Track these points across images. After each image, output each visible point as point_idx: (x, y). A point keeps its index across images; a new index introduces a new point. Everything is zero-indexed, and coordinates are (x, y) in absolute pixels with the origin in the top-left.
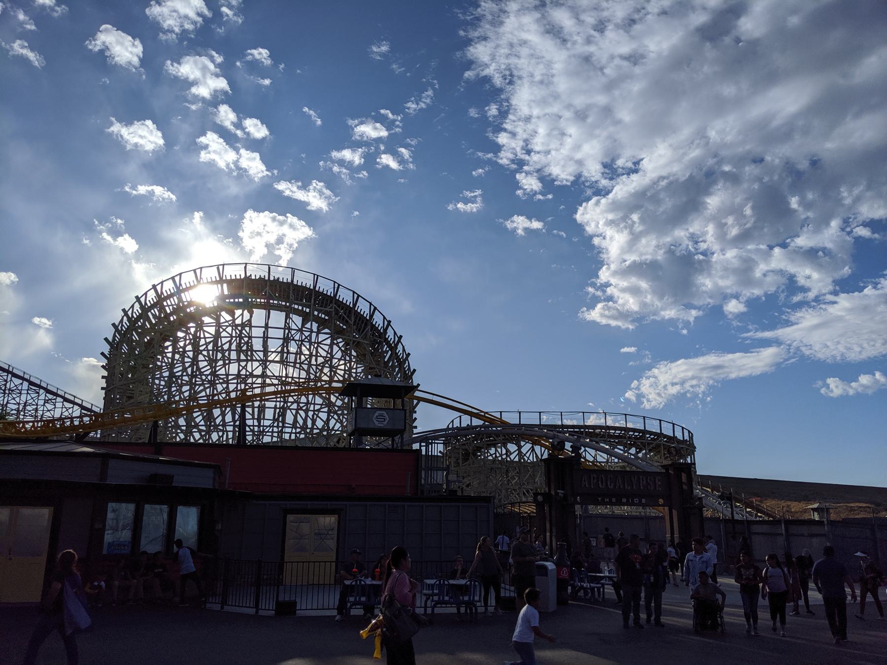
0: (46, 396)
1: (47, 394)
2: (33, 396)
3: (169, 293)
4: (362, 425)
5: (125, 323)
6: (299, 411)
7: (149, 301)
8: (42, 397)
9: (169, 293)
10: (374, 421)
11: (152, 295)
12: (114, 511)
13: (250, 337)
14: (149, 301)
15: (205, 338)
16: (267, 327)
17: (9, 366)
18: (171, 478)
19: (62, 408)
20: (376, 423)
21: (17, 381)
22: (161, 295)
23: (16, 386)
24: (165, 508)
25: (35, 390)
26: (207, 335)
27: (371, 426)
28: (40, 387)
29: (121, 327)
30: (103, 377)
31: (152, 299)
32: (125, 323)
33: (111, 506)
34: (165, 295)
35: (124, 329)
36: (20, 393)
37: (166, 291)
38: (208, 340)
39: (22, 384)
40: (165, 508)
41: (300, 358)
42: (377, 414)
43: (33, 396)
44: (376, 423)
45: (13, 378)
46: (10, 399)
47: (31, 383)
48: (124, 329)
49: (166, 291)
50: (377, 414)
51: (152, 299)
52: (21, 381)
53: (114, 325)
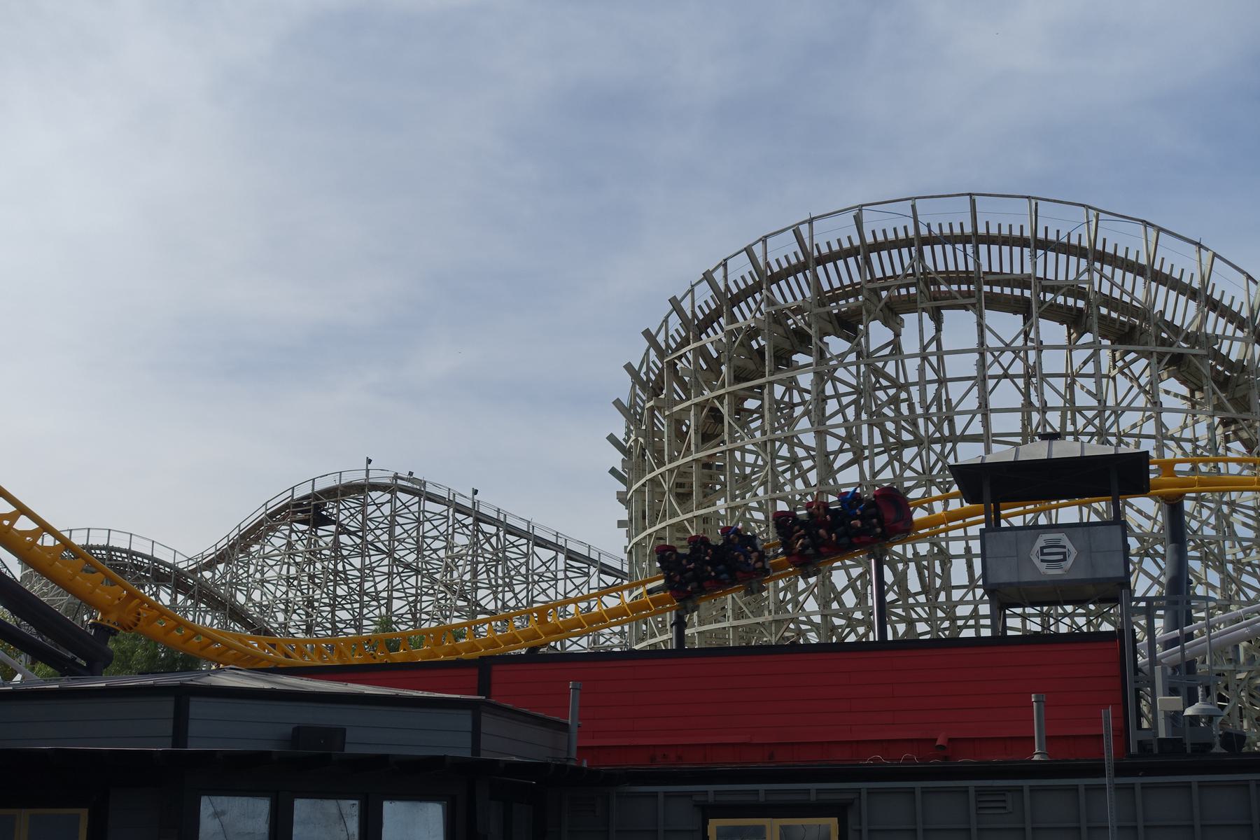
0: (600, 579)
1: (602, 576)
2: (578, 581)
3: (743, 286)
4: (1003, 575)
5: (677, 331)
6: (445, 544)
7: (700, 307)
8: (594, 582)
9: (743, 286)
10: (1037, 562)
11: (704, 294)
12: (217, 814)
13: (942, 381)
14: (700, 307)
15: (838, 396)
16: (982, 349)
17: (529, 522)
18: (338, 734)
19: (284, 593)
20: (1042, 567)
21: (546, 554)
22: (725, 294)
23: (544, 564)
24: (351, 808)
25: (579, 568)
26: (842, 389)
27: (1027, 577)
28: (589, 561)
29: (666, 341)
30: (621, 524)
31: (706, 302)
32: (677, 331)
33: (207, 805)
34: (735, 291)
35: (653, 378)
36: (556, 579)
37: (735, 282)
38: (845, 400)
39: (555, 558)
40: (351, 808)
41: (1074, 423)
42: (1040, 542)
43: (578, 581)
44: (1042, 567)
45: (536, 549)
46: (535, 593)
47: (571, 555)
48: (653, 378)
49: (735, 282)
50: (1040, 542)
51: (706, 302)
52: (553, 553)
53: (629, 367)
